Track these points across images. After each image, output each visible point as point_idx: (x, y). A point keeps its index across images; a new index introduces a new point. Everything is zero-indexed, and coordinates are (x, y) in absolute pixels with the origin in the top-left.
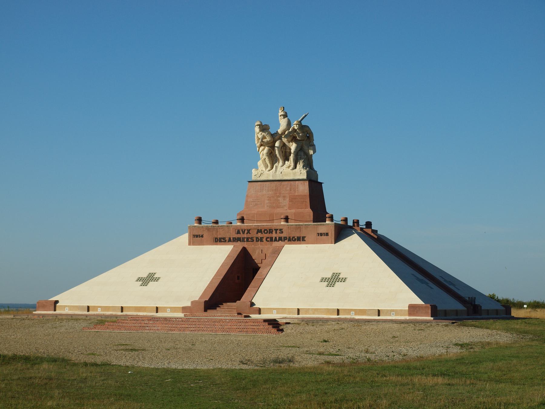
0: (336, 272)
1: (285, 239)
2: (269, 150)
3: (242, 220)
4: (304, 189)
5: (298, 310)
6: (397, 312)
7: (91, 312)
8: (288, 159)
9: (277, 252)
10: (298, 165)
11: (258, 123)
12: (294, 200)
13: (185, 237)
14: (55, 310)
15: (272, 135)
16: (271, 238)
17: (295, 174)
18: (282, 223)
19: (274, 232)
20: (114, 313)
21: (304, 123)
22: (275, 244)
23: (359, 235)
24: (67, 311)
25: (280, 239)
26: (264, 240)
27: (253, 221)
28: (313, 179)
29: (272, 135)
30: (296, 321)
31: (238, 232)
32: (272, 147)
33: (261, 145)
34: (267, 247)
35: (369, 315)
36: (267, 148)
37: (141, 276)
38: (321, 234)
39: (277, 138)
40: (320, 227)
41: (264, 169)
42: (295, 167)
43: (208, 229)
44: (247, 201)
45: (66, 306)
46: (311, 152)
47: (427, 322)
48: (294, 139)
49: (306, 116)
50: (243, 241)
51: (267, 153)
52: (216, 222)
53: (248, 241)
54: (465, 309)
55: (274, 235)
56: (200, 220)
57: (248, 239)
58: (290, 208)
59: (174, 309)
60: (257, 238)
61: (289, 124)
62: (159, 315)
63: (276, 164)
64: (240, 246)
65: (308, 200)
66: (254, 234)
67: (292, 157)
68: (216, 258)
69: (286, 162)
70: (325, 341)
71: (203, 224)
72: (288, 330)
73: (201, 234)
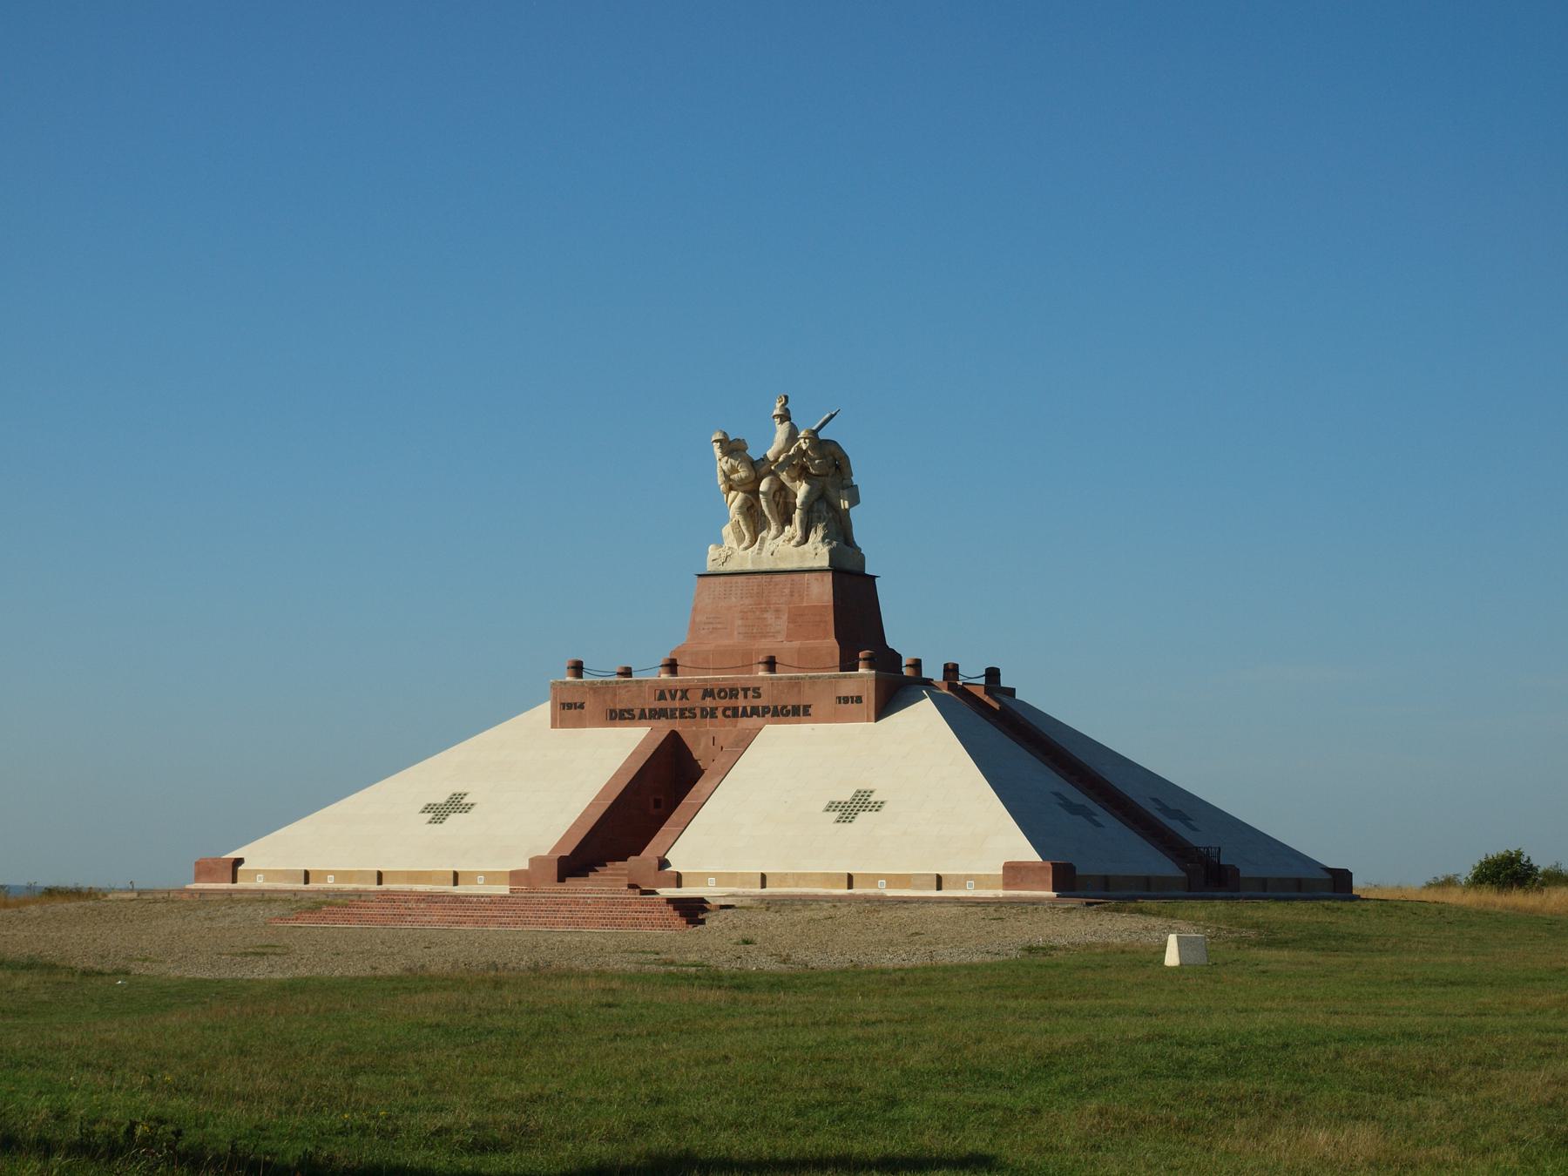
0: (863, 788)
1: (766, 710)
2: (745, 500)
3: (672, 666)
4: (822, 591)
5: (763, 876)
6: (980, 881)
7: (312, 886)
8: (789, 521)
9: (744, 742)
10: (812, 536)
11: (718, 436)
12: (799, 619)
13: (545, 710)
14: (234, 881)
15: (753, 465)
16: (735, 709)
17: (802, 556)
18: (761, 674)
19: (741, 694)
20: (361, 886)
21: (822, 435)
22: (746, 723)
23: (940, 703)
24: (260, 883)
25: (755, 711)
26: (719, 713)
27: (696, 668)
28: (848, 566)
29: (753, 465)
30: (747, 902)
31: (662, 697)
32: (754, 492)
33: (731, 489)
34: (723, 729)
35: (917, 888)
36: (741, 495)
37: (837, 799)
38: (846, 700)
39: (763, 470)
40: (844, 682)
41: (735, 545)
42: (805, 539)
43: (593, 688)
44: (693, 622)
45: (259, 871)
46: (845, 504)
47: (1035, 903)
48: (803, 473)
49: (832, 417)
50: (673, 717)
51: (741, 507)
52: (627, 672)
53: (682, 716)
54: (1184, 875)
55: (741, 702)
56: (578, 668)
57: (682, 711)
58: (789, 637)
59: (491, 877)
60: (703, 709)
61: (792, 436)
62: (460, 890)
63: (764, 533)
64: (664, 727)
65: (830, 618)
66: (695, 700)
67: (797, 516)
68: (609, 754)
69: (787, 528)
70: (747, 942)
71: (586, 678)
72: (713, 921)
73: (578, 700)
